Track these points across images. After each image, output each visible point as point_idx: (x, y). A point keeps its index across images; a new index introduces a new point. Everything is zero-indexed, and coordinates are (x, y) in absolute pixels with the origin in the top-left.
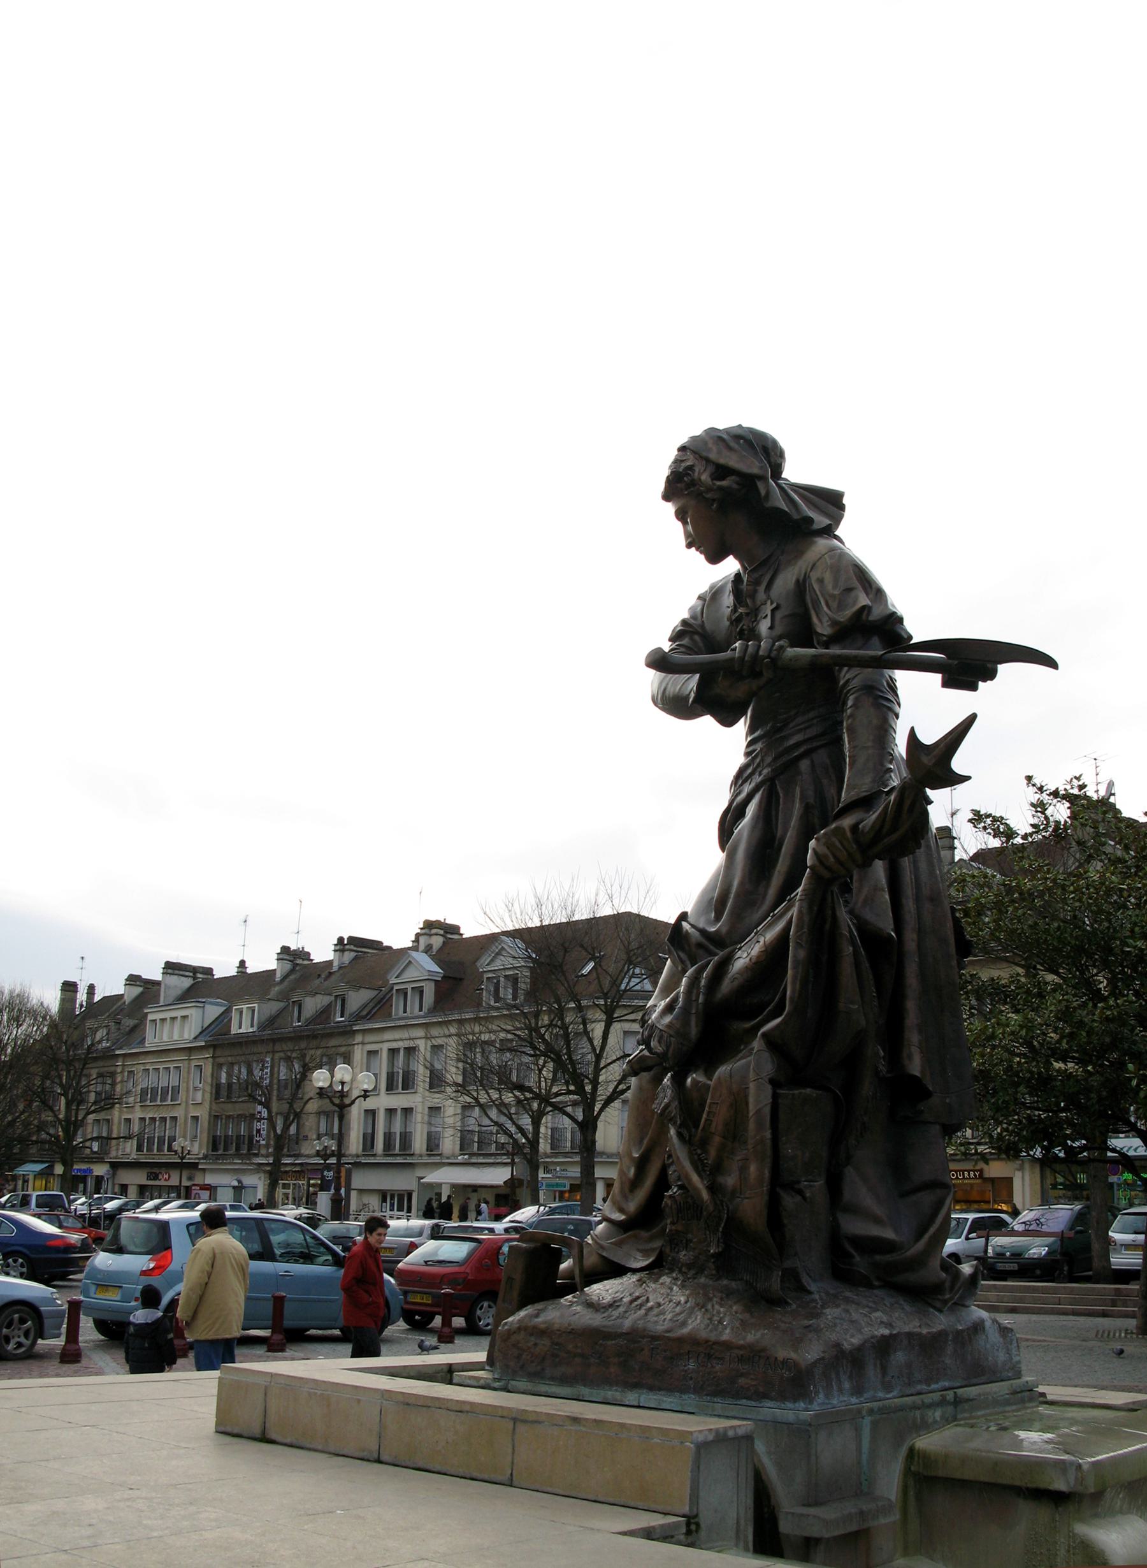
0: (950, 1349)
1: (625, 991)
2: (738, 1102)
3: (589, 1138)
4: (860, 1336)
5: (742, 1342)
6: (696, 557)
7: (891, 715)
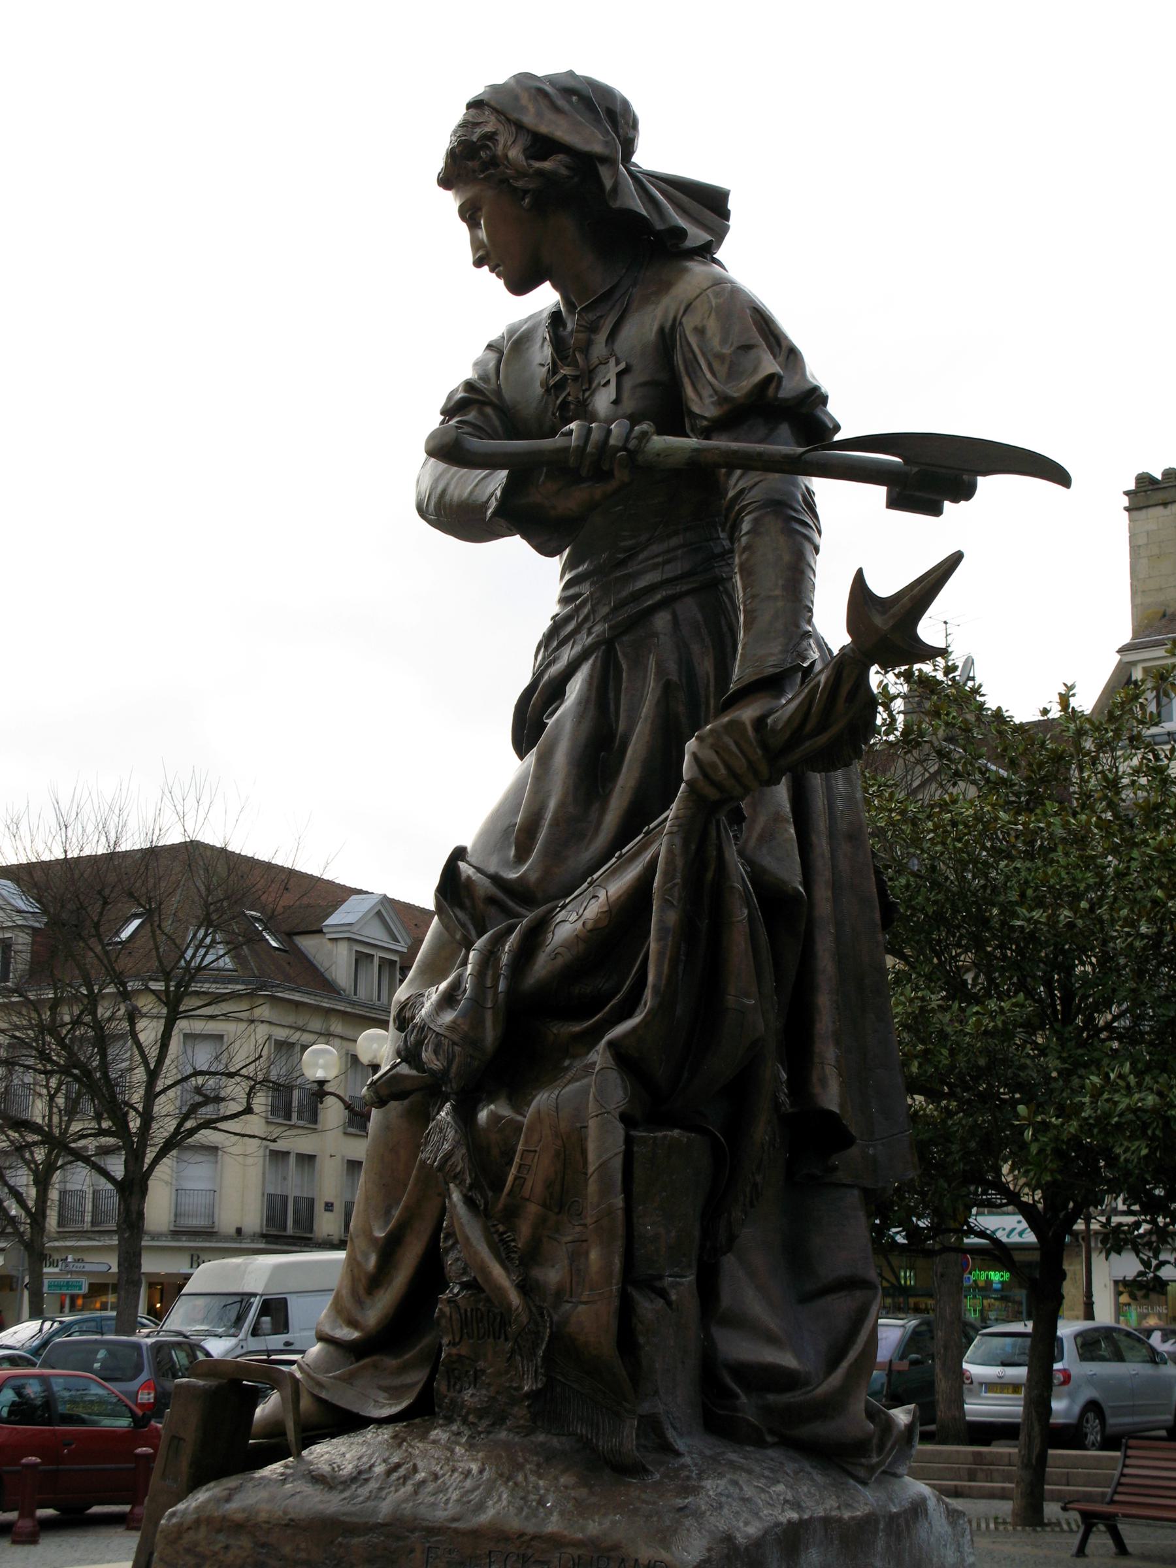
0: (880, 1544)
1: (199, 968)
2: (570, 1151)
3: (134, 1208)
4: (758, 1524)
5: (580, 1536)
6: (490, 283)
7: (808, 548)
